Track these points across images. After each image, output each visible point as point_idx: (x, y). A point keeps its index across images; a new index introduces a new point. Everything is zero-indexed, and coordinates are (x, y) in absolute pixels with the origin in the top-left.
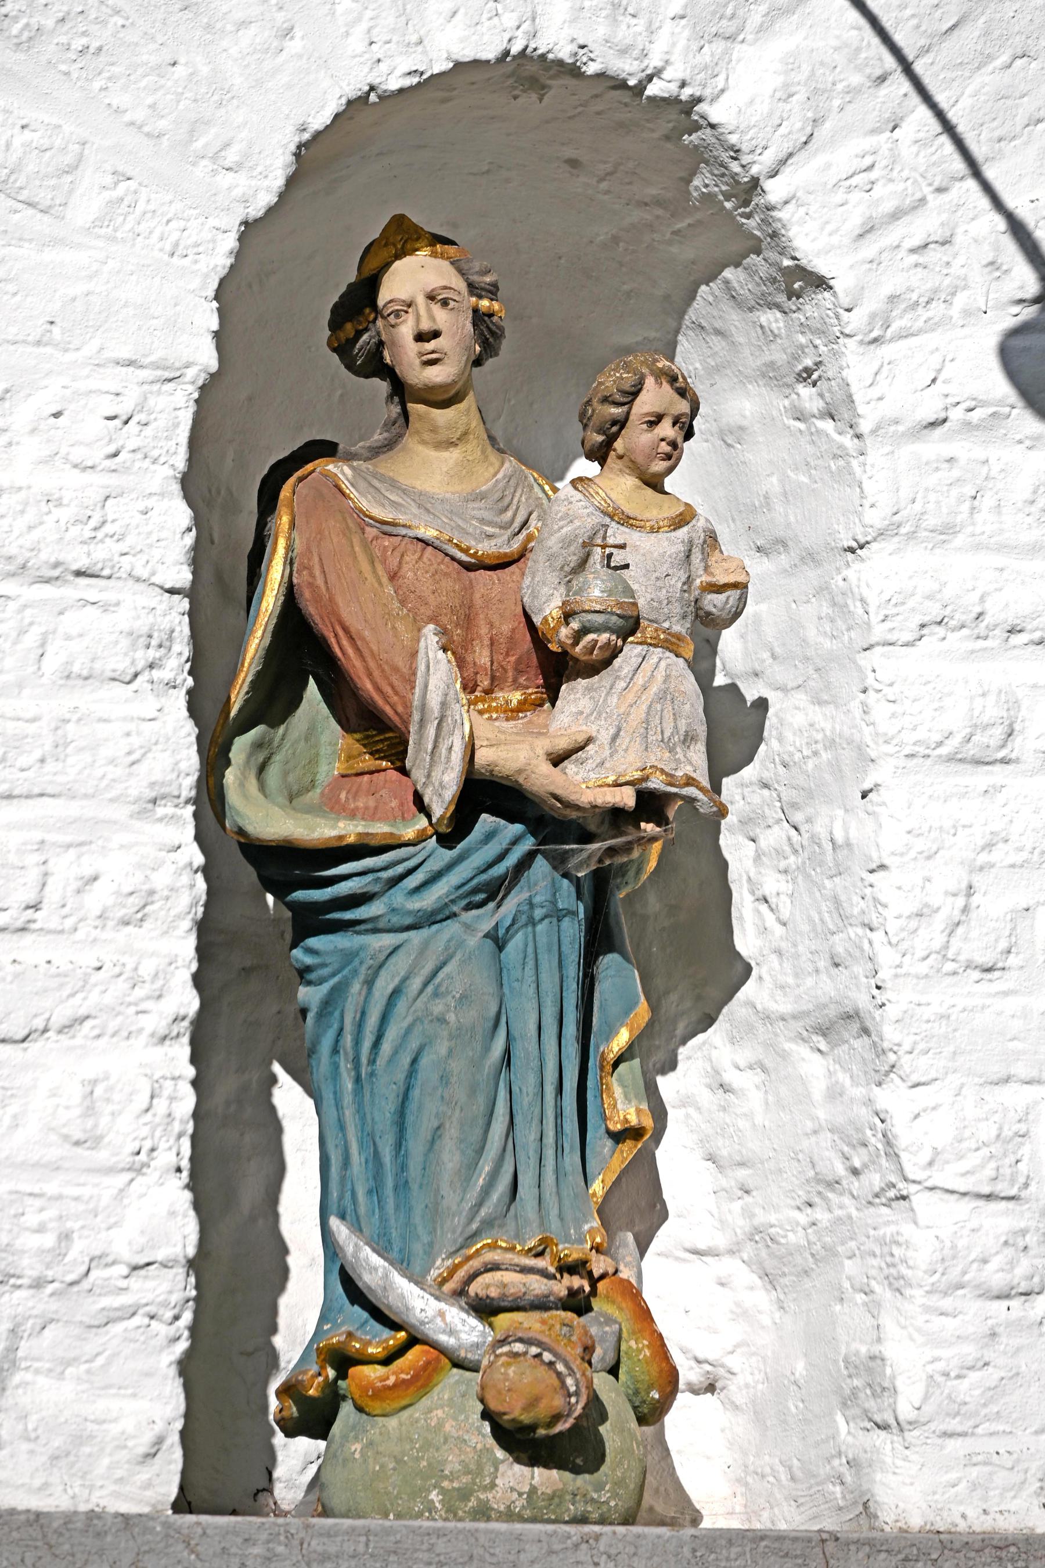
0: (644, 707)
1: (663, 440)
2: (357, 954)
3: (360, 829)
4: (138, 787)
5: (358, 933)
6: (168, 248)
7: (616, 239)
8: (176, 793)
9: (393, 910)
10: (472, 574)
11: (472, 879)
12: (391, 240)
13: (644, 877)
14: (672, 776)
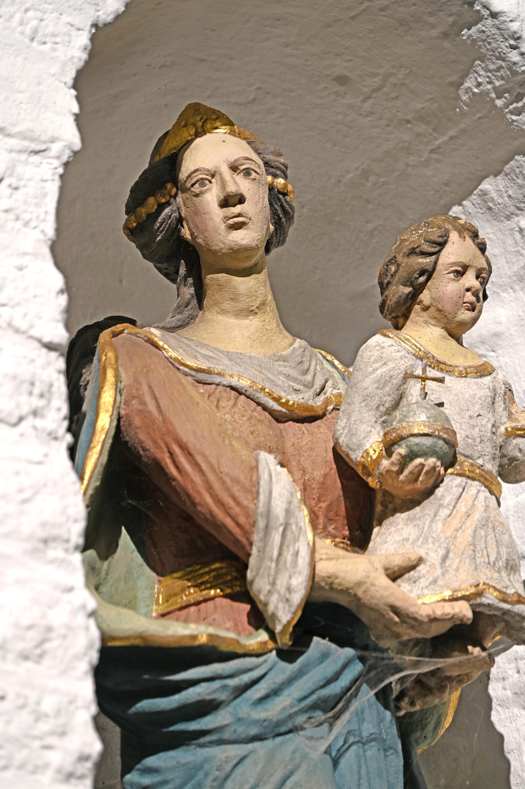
0: (470, 531)
1: (468, 290)
2: (201, 767)
3: (211, 630)
4: (29, 524)
5: (201, 746)
6: (28, 31)
7: (365, 174)
8: (65, 536)
9: (239, 720)
10: (281, 425)
11: (313, 692)
12: (191, 120)
13: (442, 732)
14: (505, 593)
